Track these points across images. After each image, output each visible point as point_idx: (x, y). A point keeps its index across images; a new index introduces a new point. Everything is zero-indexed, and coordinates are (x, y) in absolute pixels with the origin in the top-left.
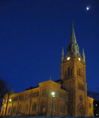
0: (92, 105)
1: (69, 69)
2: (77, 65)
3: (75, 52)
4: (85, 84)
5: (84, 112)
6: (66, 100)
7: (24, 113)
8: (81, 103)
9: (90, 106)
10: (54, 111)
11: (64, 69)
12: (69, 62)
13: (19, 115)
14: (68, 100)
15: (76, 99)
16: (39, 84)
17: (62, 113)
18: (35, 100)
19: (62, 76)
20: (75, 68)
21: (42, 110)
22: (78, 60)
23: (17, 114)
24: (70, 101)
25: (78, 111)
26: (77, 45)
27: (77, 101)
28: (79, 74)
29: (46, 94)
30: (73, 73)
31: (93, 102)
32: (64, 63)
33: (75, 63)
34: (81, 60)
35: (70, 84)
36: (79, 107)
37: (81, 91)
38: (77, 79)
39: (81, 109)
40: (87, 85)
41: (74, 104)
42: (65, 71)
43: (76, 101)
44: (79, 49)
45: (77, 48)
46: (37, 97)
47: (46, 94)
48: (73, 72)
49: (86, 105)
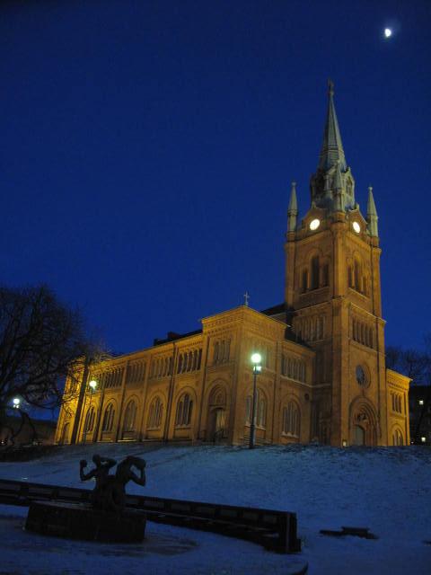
5: (375, 429)
12: (316, 237)
14: (314, 383)
17: (289, 434)
22: (351, 229)
25: (352, 424)
26: (348, 174)
28: (353, 284)
29: (228, 361)
30: (331, 283)
33: (340, 242)
34: (362, 229)
36: (356, 411)
37: (364, 347)
38: (346, 301)
39: (362, 417)
41: (335, 399)
44: (353, 187)
45: (349, 182)
48: (331, 274)
49: (383, 401)
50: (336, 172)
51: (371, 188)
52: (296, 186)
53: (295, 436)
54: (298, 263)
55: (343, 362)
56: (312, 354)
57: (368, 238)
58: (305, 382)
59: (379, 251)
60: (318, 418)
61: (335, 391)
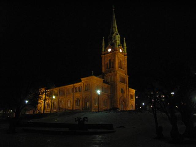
0: (133, 96)
1: (110, 61)
2: (118, 57)
5: (126, 104)
7: (66, 108)
8: (123, 96)
9: (132, 98)
11: (105, 61)
12: (110, 54)
13: (61, 110)
15: (118, 92)
16: (82, 79)
17: (105, 107)
18: (77, 95)
21: (86, 104)
22: (119, 52)
23: (59, 109)
24: (112, 94)
26: (119, 36)
27: (119, 94)
28: (120, 67)
30: (114, 67)
31: (134, 94)
32: (105, 54)
33: (116, 56)
34: (122, 51)
35: (112, 77)
37: (123, 84)
38: (118, 72)
40: (129, 78)
42: (106, 63)
43: (118, 95)
45: (119, 38)
47: (89, 89)
50: (115, 35)
51: (124, 39)
59: (127, 57)
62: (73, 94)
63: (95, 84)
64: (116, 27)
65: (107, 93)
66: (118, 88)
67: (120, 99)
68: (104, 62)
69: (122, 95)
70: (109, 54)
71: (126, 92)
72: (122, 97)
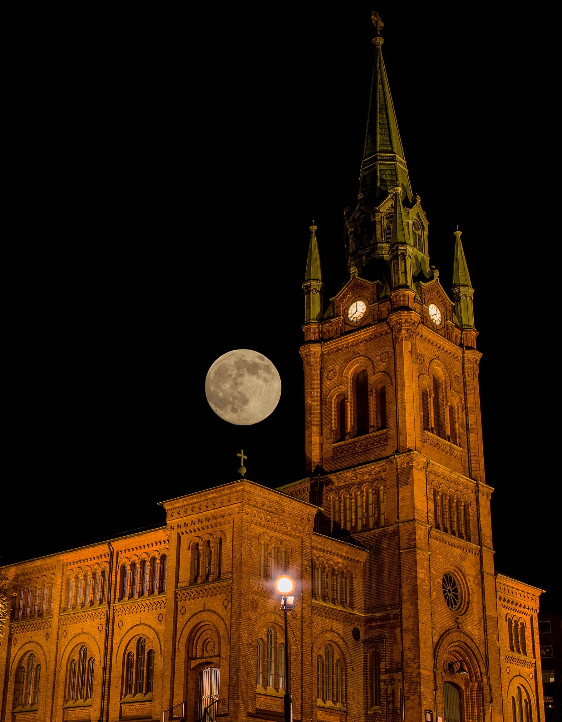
3: (401, 264)
4: (477, 492)
5: (481, 689)
6: (356, 612)
8: (458, 627)
10: (265, 687)
12: (363, 334)
14: (368, 609)
16: (168, 506)
17: (329, 704)
19: (316, 439)
20: (407, 383)
22: (425, 320)
25: (439, 682)
26: (417, 210)
28: (432, 424)
29: (219, 578)
30: (391, 422)
31: (535, 615)
32: (322, 340)
33: (406, 346)
34: (445, 317)
35: (377, 493)
36: (445, 656)
37: (456, 540)
38: (420, 460)
39: (457, 667)
41: (408, 638)
43: (424, 617)
44: (426, 233)
45: (418, 225)
46: (157, 597)
48: (390, 407)
49: (492, 637)
50: (394, 207)
51: (459, 234)
52: (317, 232)
53: (339, 705)
54: (328, 384)
55: (419, 570)
56: (363, 556)
57: (457, 331)
58: (352, 608)
59: (478, 355)
60: (378, 673)
61: (407, 623)
62: (104, 608)
63: (258, 537)
64: (400, 158)
65: (343, 603)
66: (421, 574)
67: (437, 647)
68: (316, 393)
69: (450, 623)
70: (350, 339)
71: (475, 598)
72: (455, 636)
